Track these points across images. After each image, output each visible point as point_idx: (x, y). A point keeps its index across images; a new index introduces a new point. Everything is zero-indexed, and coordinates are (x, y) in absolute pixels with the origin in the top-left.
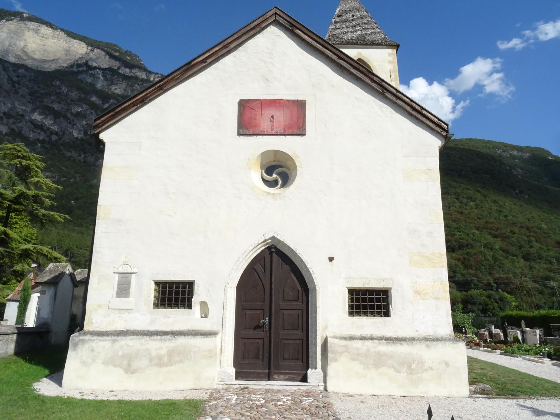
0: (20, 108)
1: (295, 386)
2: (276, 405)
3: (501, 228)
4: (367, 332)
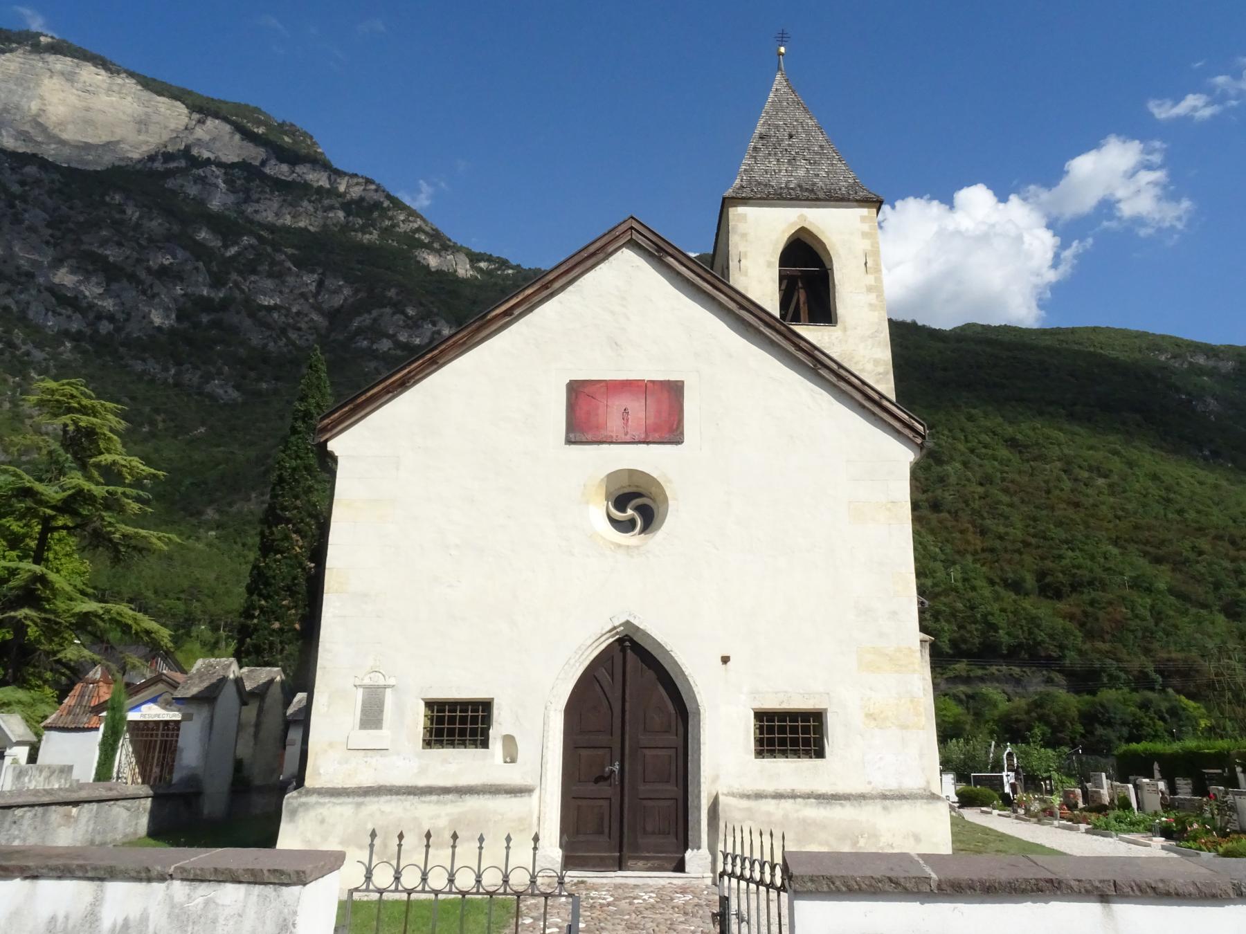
0: (24, 256)
1: (664, 879)
2: (631, 904)
3: (1170, 541)
4: (784, 786)
